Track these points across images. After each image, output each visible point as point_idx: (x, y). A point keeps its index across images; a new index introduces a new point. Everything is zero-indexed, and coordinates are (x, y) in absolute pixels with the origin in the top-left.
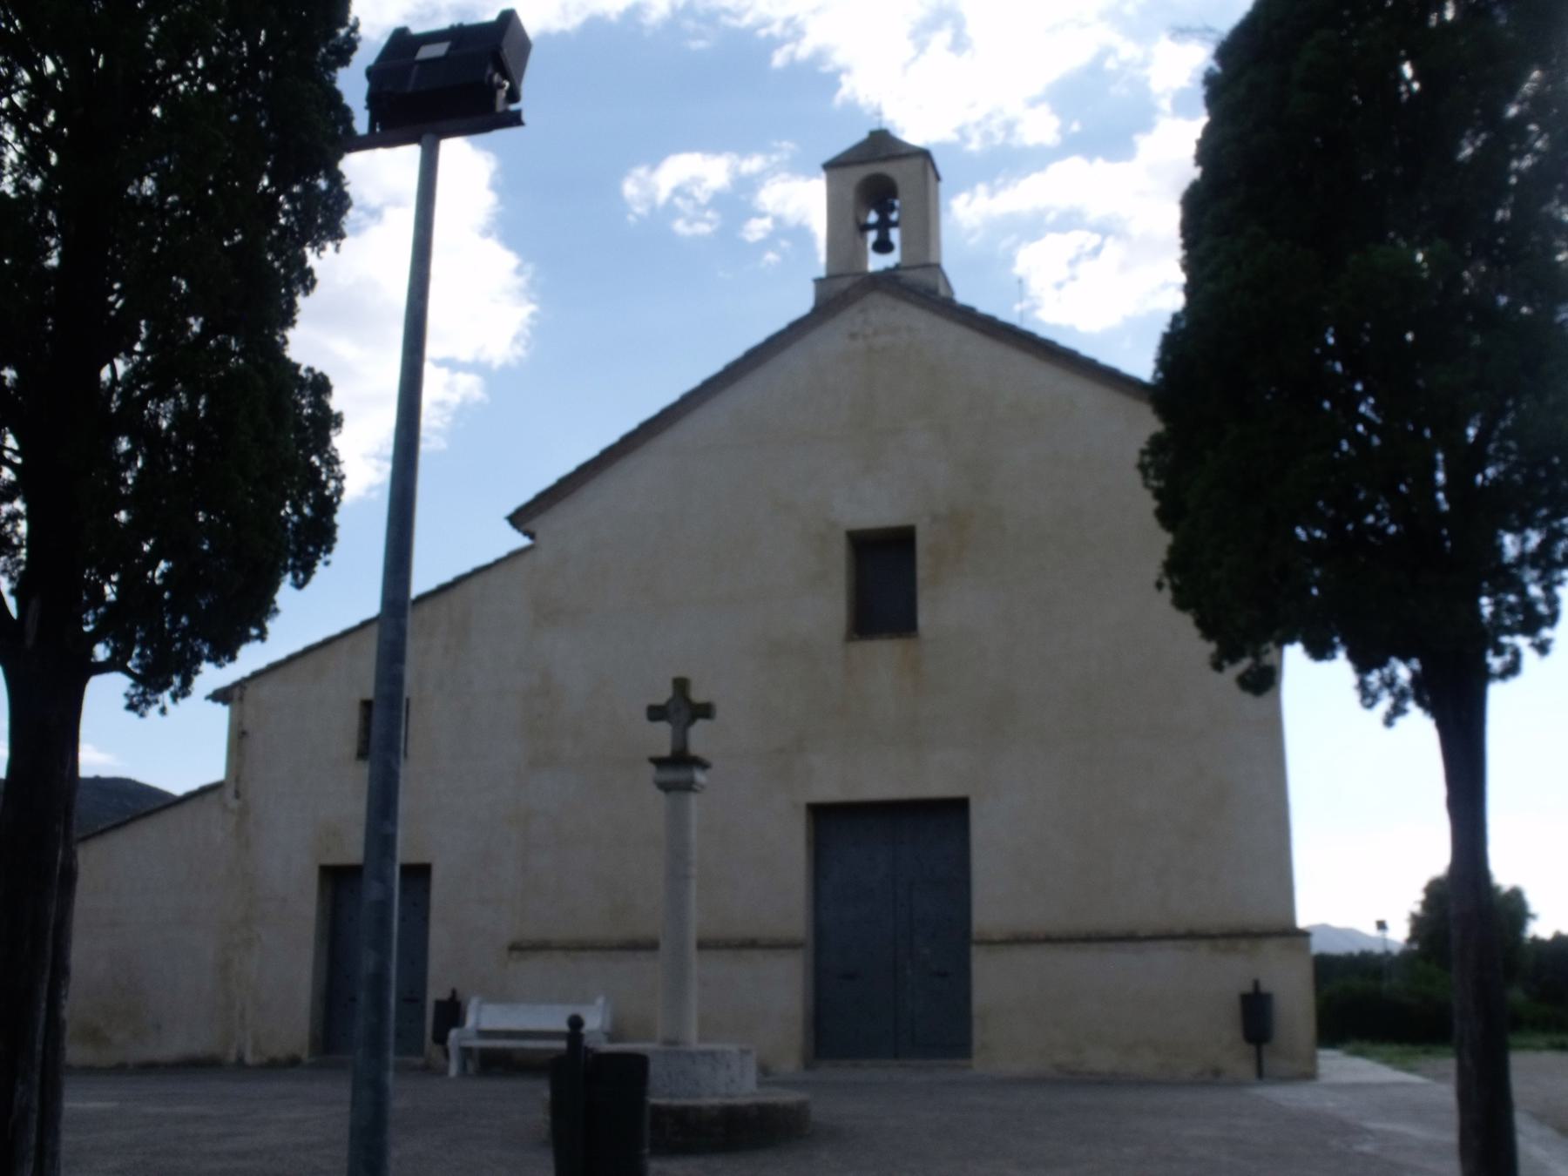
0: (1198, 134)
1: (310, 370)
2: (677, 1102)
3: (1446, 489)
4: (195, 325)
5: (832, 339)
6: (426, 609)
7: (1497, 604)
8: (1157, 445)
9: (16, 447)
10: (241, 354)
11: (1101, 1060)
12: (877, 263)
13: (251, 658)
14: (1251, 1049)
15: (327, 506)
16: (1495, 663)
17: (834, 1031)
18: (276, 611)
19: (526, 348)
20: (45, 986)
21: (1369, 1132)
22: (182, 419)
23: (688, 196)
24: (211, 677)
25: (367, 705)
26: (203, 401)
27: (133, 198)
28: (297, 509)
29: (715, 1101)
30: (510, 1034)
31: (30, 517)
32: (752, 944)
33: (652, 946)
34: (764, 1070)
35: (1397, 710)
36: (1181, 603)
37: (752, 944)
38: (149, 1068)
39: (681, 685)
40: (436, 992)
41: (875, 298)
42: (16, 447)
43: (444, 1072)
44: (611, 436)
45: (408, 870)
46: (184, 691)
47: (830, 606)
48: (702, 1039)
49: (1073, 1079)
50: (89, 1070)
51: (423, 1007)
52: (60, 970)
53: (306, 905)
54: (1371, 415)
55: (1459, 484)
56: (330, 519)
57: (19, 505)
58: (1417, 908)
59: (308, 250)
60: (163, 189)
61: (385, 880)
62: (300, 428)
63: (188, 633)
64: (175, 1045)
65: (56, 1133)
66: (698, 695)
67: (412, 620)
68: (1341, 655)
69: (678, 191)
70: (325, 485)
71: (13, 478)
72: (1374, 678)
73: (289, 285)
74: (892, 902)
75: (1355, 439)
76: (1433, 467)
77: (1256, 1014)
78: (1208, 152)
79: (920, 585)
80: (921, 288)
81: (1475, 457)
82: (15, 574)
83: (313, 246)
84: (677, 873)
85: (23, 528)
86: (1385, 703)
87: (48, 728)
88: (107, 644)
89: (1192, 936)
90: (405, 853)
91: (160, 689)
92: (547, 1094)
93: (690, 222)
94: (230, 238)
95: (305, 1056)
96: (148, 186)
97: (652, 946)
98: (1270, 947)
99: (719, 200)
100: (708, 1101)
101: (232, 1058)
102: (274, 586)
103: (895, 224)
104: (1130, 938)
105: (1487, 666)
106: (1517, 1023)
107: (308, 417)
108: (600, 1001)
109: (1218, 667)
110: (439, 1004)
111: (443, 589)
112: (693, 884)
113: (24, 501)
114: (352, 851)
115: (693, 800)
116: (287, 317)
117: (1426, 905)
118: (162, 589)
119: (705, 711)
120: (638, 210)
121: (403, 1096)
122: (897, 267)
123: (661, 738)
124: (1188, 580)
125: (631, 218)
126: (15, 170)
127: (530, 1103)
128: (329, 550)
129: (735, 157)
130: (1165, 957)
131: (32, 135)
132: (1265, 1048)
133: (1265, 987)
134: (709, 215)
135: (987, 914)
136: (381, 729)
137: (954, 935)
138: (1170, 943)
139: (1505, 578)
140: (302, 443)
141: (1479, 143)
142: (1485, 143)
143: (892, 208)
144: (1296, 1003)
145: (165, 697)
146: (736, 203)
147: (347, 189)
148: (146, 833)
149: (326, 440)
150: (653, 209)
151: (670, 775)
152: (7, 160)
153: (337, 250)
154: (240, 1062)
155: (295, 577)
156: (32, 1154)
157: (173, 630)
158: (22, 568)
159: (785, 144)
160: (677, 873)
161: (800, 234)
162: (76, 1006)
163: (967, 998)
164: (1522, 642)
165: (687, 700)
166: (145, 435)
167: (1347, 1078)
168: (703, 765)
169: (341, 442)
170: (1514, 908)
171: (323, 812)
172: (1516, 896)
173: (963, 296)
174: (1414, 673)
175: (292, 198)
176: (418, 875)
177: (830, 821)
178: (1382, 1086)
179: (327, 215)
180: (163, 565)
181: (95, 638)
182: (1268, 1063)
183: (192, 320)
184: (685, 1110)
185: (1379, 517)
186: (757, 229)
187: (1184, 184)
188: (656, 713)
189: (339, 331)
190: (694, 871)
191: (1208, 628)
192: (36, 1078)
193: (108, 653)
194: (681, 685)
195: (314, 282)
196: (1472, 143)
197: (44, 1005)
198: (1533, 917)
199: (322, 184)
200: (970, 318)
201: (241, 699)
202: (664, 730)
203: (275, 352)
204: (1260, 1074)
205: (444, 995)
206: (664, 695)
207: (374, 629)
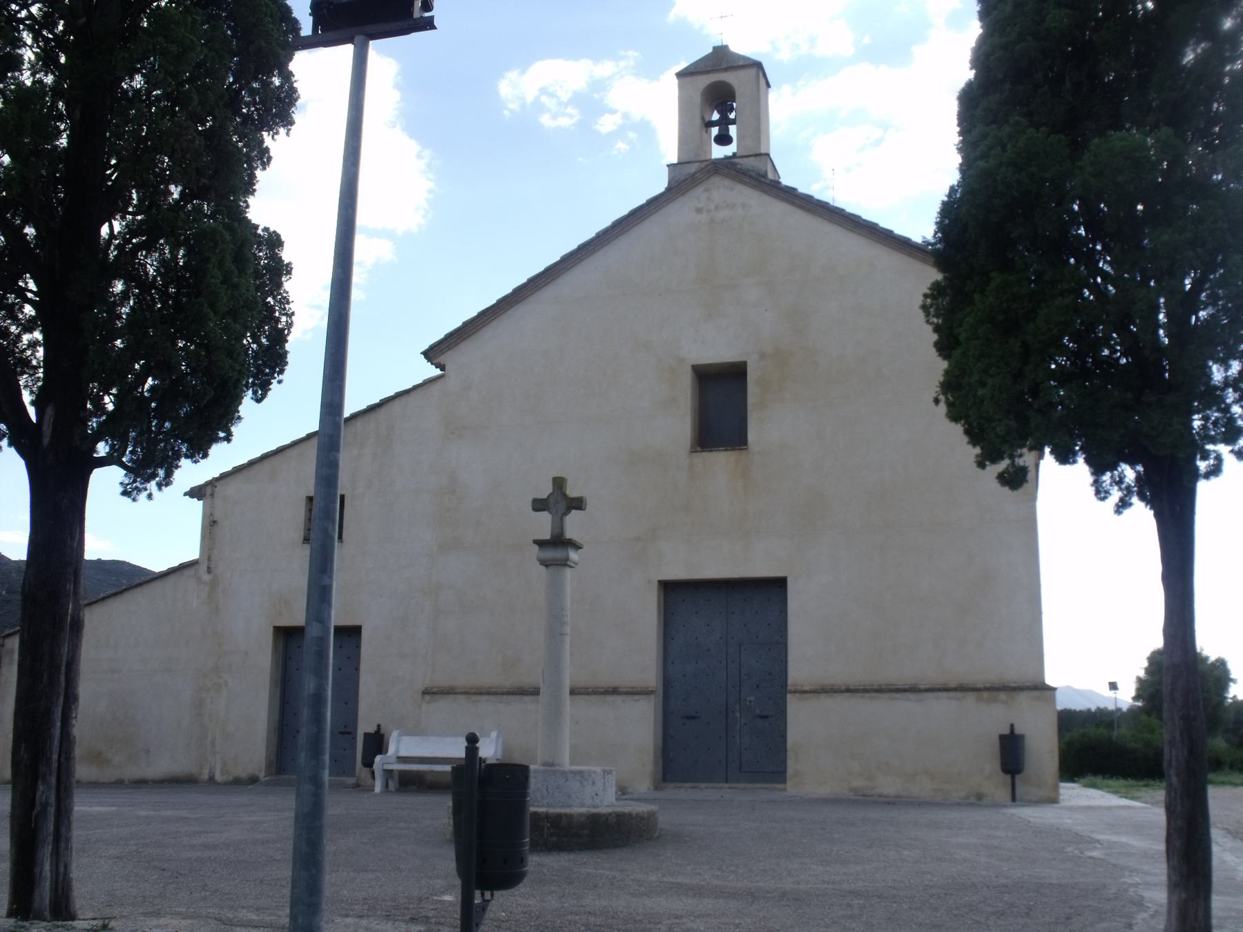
0: (972, 43)
1: (266, 229)
2: (552, 810)
3: (1168, 327)
4: (175, 191)
5: (682, 212)
6: (358, 423)
7: (1206, 419)
8: (937, 291)
9: (35, 289)
10: (212, 216)
11: (888, 786)
12: (718, 152)
13: (222, 458)
14: (1008, 777)
15: (279, 338)
16: (1202, 465)
17: (677, 761)
18: (239, 418)
19: (424, 217)
20: (60, 709)
21: (1098, 841)
22: (166, 267)
23: (552, 95)
24: (190, 473)
25: (310, 499)
26: (181, 252)
27: (126, 91)
28: (256, 339)
29: (583, 810)
30: (422, 760)
31: (46, 345)
32: (614, 691)
33: (535, 692)
34: (622, 791)
35: (1123, 505)
36: (954, 416)
37: (614, 691)
38: (140, 783)
39: (559, 483)
40: (365, 726)
41: (716, 180)
42: (35, 289)
43: (372, 788)
44: (506, 288)
45: (339, 630)
46: (166, 482)
47: (679, 424)
48: (572, 764)
49: (865, 799)
50: (94, 785)
51: (355, 738)
52: (71, 697)
53: (263, 657)
54: (1107, 268)
55: (1178, 324)
56: (283, 347)
57: (38, 335)
58: (1142, 674)
59: (265, 134)
60: (151, 83)
61: (323, 640)
62: (258, 275)
63: (173, 434)
65: (69, 829)
66: (572, 492)
67: (345, 434)
68: (1081, 459)
69: (543, 91)
70: (278, 320)
71: (33, 313)
72: (1107, 477)
73: (250, 161)
74: (725, 668)
75: (1095, 289)
76: (1156, 311)
77: (1011, 752)
78: (984, 58)
79: (749, 408)
80: (752, 172)
81: (1190, 302)
82: (35, 389)
83: (268, 131)
84: (555, 632)
85: (40, 352)
86: (1116, 495)
87: (57, 510)
88: (107, 441)
89: (962, 689)
90: (338, 616)
91: (148, 480)
92: (450, 804)
93: (554, 117)
94: (203, 125)
95: (262, 775)
96: (138, 81)
97: (535, 692)
98: (1023, 698)
99: (578, 100)
100: (576, 810)
101: (205, 777)
102: (238, 400)
103: (733, 122)
104: (913, 689)
105: (1197, 468)
106: (1217, 764)
107: (265, 267)
108: (494, 734)
109: (981, 465)
110: (366, 735)
111: (372, 409)
112: (568, 639)
113: (41, 332)
114: (297, 616)
115: (568, 572)
116: (248, 187)
117: (1148, 671)
118: (150, 400)
119: (578, 504)
120: (511, 106)
121: (336, 807)
122: (734, 155)
123: (543, 525)
124: (961, 398)
125: (505, 112)
126: (33, 66)
127: (438, 812)
128: (281, 372)
129: (589, 62)
130: (941, 705)
131: (46, 40)
132: (1017, 777)
133: (1018, 731)
134: (570, 110)
135: (799, 670)
136: (324, 519)
137: (773, 687)
138: (944, 694)
139: (1212, 397)
140: (258, 288)
141: (1199, 51)
142: (1204, 50)
143: (732, 109)
144: (1043, 748)
145: (152, 485)
146: (590, 103)
147: (295, 85)
148: (138, 598)
149: (279, 285)
150: (523, 106)
151: (550, 554)
152: (26, 58)
153: (288, 134)
154: (212, 779)
155: (255, 393)
156: (51, 839)
157: (159, 432)
158: (40, 384)
159: (630, 53)
160: (555, 632)
161: (644, 129)
162: (81, 729)
163: (783, 736)
164: (1223, 449)
165: (565, 495)
166: (134, 277)
167: (1084, 802)
168: (576, 546)
169: (290, 286)
170: (1219, 675)
171: (274, 586)
172: (1221, 665)
173: (786, 180)
174: (1138, 473)
175: (253, 92)
176: (350, 634)
178: (1110, 808)
179: (279, 108)
180: (150, 381)
181: (98, 436)
182: (1019, 790)
183: (172, 188)
184: (559, 816)
185: (1113, 351)
186: (607, 124)
187: (961, 84)
188: (539, 505)
189: (288, 195)
190: (568, 629)
191: (974, 436)
192: (53, 780)
193: (107, 449)
194: (559, 483)
195: (270, 159)
196: (1194, 50)
197: (59, 724)
198: (1234, 681)
199: (277, 81)
200: (791, 196)
201: (212, 495)
202: (545, 518)
203: (237, 217)
204: (1014, 799)
205: (372, 729)
206: (545, 490)
207: (315, 441)
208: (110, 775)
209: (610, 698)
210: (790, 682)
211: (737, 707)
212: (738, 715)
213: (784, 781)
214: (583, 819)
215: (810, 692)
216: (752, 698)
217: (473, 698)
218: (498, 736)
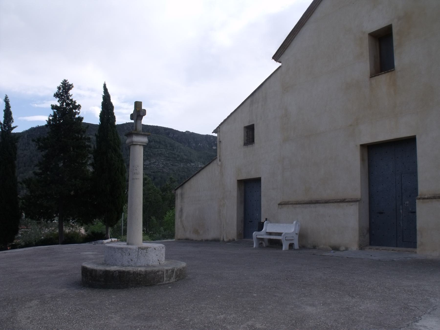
37: (343, 201)
38: (207, 241)
47: (364, 66)
64: (211, 235)
79: (394, 48)
101: (222, 239)
135: (425, 185)
137: (413, 192)
177: (371, 150)
208: (199, 238)
209: (341, 204)
210: (419, 193)
211: (401, 207)
212: (401, 211)
213: (415, 247)
214: (101, 273)
215: (427, 198)
216: (408, 202)
217: (294, 206)
218: (296, 223)
